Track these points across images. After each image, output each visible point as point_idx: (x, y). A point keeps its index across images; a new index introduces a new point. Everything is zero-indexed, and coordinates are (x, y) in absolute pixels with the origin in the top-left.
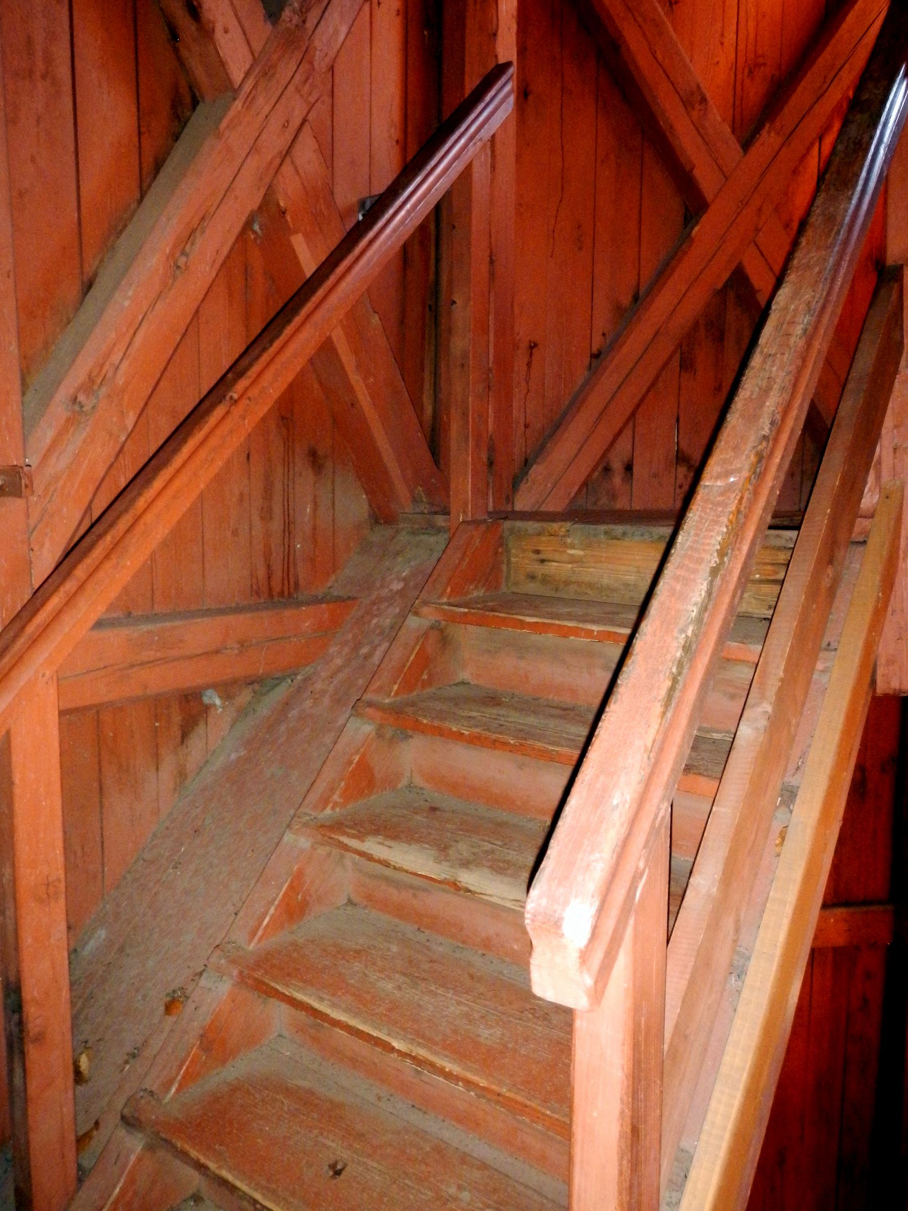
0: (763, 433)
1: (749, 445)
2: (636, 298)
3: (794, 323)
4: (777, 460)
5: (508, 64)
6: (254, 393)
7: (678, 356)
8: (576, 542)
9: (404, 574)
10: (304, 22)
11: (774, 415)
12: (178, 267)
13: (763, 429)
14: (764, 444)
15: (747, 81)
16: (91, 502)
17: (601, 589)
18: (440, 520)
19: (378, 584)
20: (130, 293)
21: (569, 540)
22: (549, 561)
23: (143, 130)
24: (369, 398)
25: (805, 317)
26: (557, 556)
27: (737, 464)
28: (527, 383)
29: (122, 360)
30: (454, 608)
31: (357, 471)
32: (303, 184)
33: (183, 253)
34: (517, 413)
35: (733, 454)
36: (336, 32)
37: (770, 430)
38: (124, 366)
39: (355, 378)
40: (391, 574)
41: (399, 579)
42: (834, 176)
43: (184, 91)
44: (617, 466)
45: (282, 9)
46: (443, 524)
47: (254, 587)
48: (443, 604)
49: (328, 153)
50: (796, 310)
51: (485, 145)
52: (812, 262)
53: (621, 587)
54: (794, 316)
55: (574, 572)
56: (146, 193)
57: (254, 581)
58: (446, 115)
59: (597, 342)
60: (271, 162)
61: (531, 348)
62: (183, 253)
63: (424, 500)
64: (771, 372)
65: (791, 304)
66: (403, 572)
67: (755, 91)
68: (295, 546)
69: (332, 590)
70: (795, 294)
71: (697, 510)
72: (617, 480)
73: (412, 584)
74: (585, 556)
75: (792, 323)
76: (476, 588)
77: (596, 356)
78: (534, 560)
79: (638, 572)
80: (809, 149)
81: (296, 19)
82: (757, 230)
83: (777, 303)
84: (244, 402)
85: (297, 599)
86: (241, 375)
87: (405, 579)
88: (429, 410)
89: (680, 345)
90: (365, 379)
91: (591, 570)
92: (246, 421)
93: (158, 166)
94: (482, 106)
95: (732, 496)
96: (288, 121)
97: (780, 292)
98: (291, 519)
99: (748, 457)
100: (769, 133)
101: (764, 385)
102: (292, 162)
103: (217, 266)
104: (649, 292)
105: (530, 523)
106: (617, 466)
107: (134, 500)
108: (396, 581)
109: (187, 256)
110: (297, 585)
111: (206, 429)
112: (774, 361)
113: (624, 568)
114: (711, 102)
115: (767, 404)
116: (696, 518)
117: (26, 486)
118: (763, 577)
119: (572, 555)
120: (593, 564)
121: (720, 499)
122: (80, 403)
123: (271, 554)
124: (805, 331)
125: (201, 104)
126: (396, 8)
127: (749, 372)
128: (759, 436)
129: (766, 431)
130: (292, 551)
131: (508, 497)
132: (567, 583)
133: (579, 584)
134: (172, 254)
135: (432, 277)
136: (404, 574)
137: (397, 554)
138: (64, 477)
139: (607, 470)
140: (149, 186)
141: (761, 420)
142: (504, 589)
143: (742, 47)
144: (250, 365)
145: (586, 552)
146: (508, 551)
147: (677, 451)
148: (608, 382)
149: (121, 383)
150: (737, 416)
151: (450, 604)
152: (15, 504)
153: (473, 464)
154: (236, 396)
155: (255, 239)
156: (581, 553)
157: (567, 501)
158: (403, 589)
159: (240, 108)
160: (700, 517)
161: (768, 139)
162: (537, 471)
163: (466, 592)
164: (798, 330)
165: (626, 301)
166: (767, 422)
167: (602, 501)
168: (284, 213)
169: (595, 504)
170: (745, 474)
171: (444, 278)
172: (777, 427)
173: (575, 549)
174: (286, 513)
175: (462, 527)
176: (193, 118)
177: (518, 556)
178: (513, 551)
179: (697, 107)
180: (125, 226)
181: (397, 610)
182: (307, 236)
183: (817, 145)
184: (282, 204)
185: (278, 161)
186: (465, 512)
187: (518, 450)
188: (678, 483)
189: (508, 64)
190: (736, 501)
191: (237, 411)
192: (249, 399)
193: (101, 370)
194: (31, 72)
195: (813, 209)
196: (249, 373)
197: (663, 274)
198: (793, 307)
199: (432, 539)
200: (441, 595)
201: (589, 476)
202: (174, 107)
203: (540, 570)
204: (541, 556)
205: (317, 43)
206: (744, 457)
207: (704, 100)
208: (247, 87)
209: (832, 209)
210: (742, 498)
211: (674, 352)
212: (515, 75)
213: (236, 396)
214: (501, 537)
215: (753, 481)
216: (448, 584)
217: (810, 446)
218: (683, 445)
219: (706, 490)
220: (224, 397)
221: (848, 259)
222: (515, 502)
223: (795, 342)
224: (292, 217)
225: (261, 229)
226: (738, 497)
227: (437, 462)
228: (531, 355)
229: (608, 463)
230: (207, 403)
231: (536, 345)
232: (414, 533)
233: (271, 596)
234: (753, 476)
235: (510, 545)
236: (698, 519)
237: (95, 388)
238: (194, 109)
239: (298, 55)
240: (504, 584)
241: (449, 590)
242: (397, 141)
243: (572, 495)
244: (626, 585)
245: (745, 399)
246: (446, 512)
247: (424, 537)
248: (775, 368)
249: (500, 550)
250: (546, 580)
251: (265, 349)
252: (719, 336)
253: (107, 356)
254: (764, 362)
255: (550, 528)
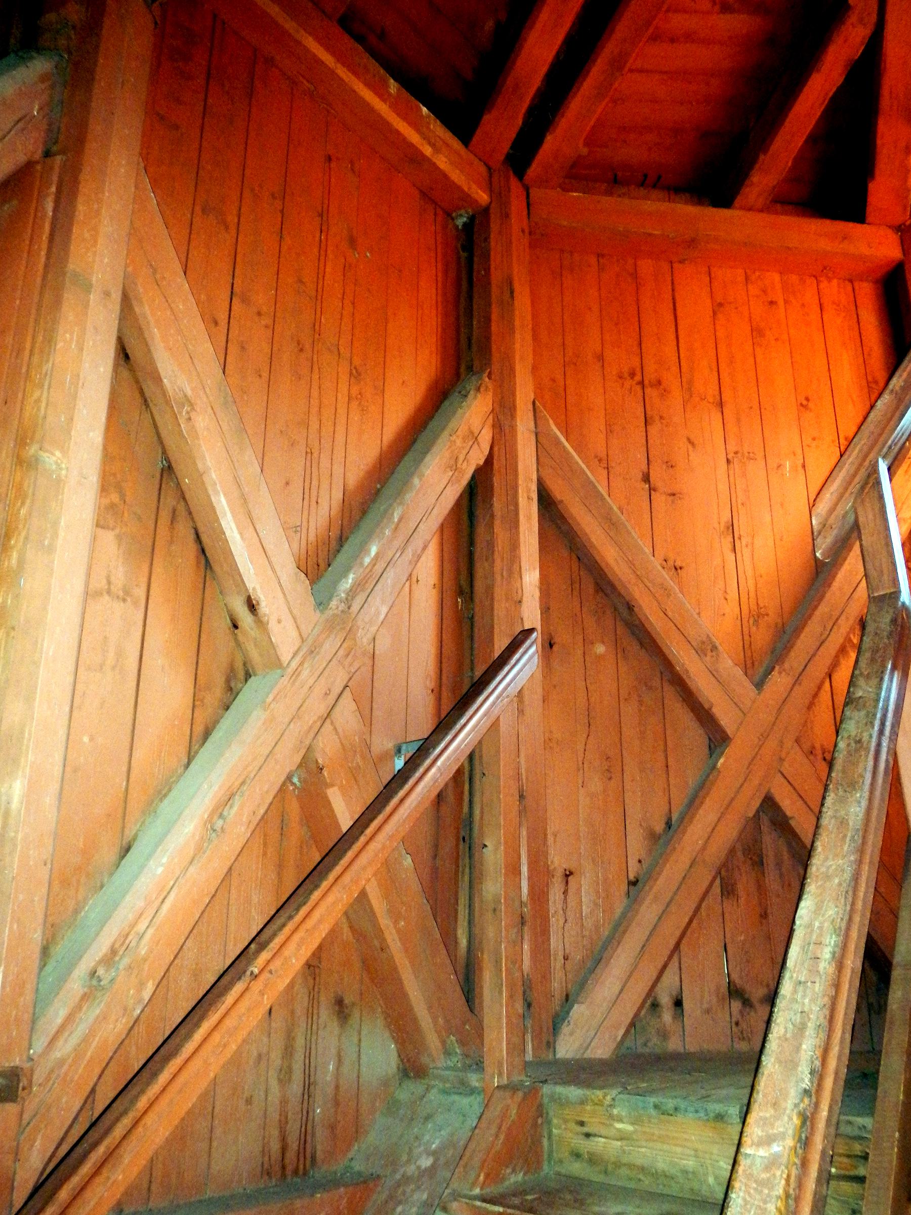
0: (804, 1086)
1: (789, 1102)
2: (669, 825)
3: (821, 943)
4: (824, 1114)
5: (531, 631)
6: (276, 964)
7: (718, 881)
8: (624, 1114)
9: (434, 1146)
10: (349, 608)
11: (812, 1062)
12: (214, 831)
13: (803, 1080)
14: (806, 1101)
15: (754, 629)
16: (96, 1084)
17: (656, 1175)
18: (474, 1080)
19: (405, 1158)
20: (164, 860)
21: (615, 1111)
22: (595, 1135)
23: (197, 703)
24: (399, 944)
25: (831, 938)
26: (603, 1132)
27: (779, 1128)
28: (565, 913)
29: (148, 927)
30: (488, 1206)
31: (385, 1019)
32: (342, 744)
33: (221, 816)
34: (555, 942)
35: (772, 1112)
36: (378, 613)
37: (812, 1083)
38: (150, 931)
39: (385, 922)
40: (420, 1145)
41: (429, 1153)
42: (840, 775)
43: (239, 665)
44: (665, 1000)
45: (330, 599)
46: (477, 1084)
47: (266, 1166)
48: (475, 1198)
49: (367, 715)
50: (821, 928)
51: (512, 701)
52: (831, 871)
53: (679, 1174)
54: (821, 935)
55: (624, 1151)
56: (194, 757)
57: (266, 1159)
58: (478, 673)
59: (633, 870)
60: (311, 728)
61: (567, 876)
62: (221, 816)
63: (458, 1051)
64: (804, 1004)
65: (815, 919)
66: (433, 1143)
67: (762, 637)
68: (314, 1111)
69: (353, 1164)
70: (818, 909)
71: (740, 1190)
72: (667, 1016)
73: (442, 1160)
74: (635, 1131)
75: (819, 943)
76: (514, 1171)
77: (634, 883)
78: (577, 1134)
79: (696, 1156)
80: (820, 688)
81: (342, 606)
82: (781, 760)
83: (801, 917)
84: (266, 975)
85: (313, 1177)
86: (262, 947)
87: (434, 1153)
88: (463, 942)
89: (719, 872)
90: (396, 923)
91: (643, 1150)
92: (266, 997)
93: (207, 734)
94: (506, 669)
95: (778, 1173)
96: (329, 690)
97: (802, 904)
98: (312, 1080)
99: (790, 1119)
100: (780, 673)
101: (798, 1021)
102: (332, 723)
103: (252, 827)
104: (682, 819)
105: (572, 1088)
106: (665, 1000)
107: (136, 1098)
108: (424, 1156)
109: (224, 819)
110: (313, 1158)
111: (222, 1009)
112: (804, 991)
113: (679, 1150)
114: (720, 648)
115: (804, 1047)
116: (740, 1201)
117: (24, 1089)
118: (843, 1172)
119: (619, 1130)
120: (644, 1144)
121: (764, 1176)
122: (99, 977)
123: (287, 1123)
124: (834, 953)
125: (253, 678)
126: (433, 583)
127: (781, 1002)
128: (800, 1091)
129: (806, 1083)
130: (311, 1117)
131: (548, 1043)
132: (618, 1165)
133: (630, 1166)
134: (210, 819)
135: (466, 809)
136: (434, 1146)
137: (428, 1118)
138: (70, 1061)
139: (655, 1006)
140: (197, 752)
141: (800, 1069)
142: (546, 1169)
143: (744, 599)
144: (274, 935)
145: (636, 1127)
146: (549, 1122)
147: (729, 983)
148: (648, 912)
149: (143, 952)
150: (773, 1060)
151: (484, 1200)
152: (11, 1108)
153: (507, 1016)
154: (256, 971)
155: (294, 790)
156: (630, 1128)
157: (614, 1045)
158: (433, 1167)
159: (285, 683)
160: (744, 1200)
161: (779, 681)
162: (578, 1011)
163: (503, 1178)
164: (826, 954)
165: (659, 827)
166: (807, 1071)
167: (652, 1043)
168: (321, 769)
169: (645, 1045)
170: (790, 1142)
171: (477, 812)
172: (818, 1075)
173: (623, 1123)
174: (307, 1072)
175: (498, 1094)
176: (244, 689)
177: (560, 1128)
178: (555, 1121)
179: (709, 654)
180: (170, 790)
181: (425, 1196)
182: (341, 787)
183: (827, 684)
184: (320, 761)
185: (319, 724)
186: (500, 1074)
187: (557, 985)
188: (734, 1020)
189: (531, 631)
190: (783, 1182)
191: (257, 986)
192: (271, 972)
193: (124, 942)
194: (101, 666)
195: (824, 810)
196: (272, 945)
197: (693, 803)
198: (817, 924)
199: (465, 1101)
200: (473, 1185)
201: (636, 1015)
202: (228, 681)
203: (585, 1146)
204: (585, 1129)
205: (360, 623)
206: (786, 1118)
207: (714, 648)
208: (294, 664)
209: (843, 813)
210: (789, 1176)
211: (714, 879)
212: (540, 640)
213: (256, 971)
214: (540, 1106)
215: (800, 1151)
216: (482, 1168)
217: (873, 977)
218: (735, 976)
219: (748, 1161)
220: (245, 972)
221: (868, 861)
222: (557, 1047)
223: (825, 968)
224: (329, 773)
225: (300, 781)
226: (785, 1176)
227: (471, 1011)
228: (567, 882)
229: (655, 998)
230: (226, 978)
231: (571, 873)
232: (445, 1092)
233: (284, 1176)
234: (798, 1145)
235: (551, 1113)
236: (743, 1203)
237: (117, 958)
238: (246, 681)
239: (342, 636)
240: (546, 1163)
241: (482, 1178)
242: (432, 691)
243: (619, 1038)
244: (685, 1172)
245: (779, 1038)
246: (479, 1065)
247: (456, 1098)
248: (807, 1001)
249: (540, 1121)
250: (593, 1160)
251: (290, 918)
252: (758, 862)
253: (133, 925)
254: (795, 991)
255: (593, 1097)
